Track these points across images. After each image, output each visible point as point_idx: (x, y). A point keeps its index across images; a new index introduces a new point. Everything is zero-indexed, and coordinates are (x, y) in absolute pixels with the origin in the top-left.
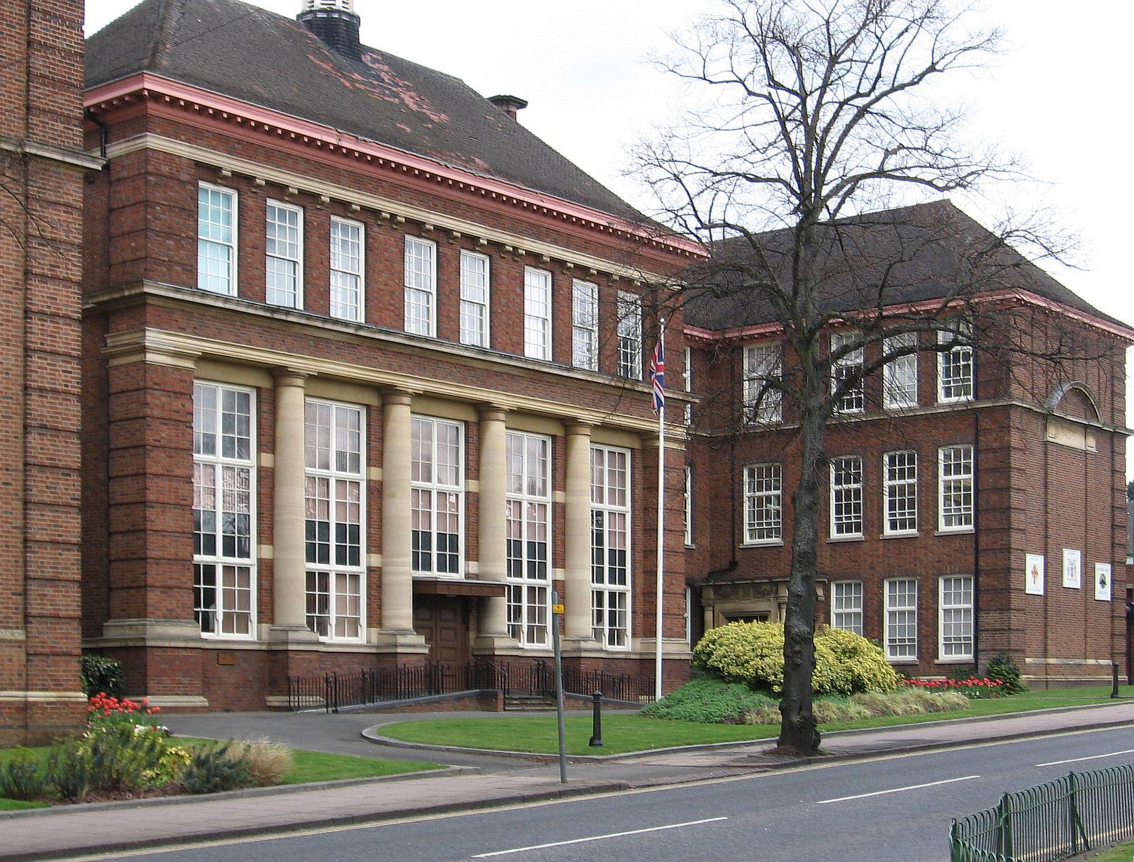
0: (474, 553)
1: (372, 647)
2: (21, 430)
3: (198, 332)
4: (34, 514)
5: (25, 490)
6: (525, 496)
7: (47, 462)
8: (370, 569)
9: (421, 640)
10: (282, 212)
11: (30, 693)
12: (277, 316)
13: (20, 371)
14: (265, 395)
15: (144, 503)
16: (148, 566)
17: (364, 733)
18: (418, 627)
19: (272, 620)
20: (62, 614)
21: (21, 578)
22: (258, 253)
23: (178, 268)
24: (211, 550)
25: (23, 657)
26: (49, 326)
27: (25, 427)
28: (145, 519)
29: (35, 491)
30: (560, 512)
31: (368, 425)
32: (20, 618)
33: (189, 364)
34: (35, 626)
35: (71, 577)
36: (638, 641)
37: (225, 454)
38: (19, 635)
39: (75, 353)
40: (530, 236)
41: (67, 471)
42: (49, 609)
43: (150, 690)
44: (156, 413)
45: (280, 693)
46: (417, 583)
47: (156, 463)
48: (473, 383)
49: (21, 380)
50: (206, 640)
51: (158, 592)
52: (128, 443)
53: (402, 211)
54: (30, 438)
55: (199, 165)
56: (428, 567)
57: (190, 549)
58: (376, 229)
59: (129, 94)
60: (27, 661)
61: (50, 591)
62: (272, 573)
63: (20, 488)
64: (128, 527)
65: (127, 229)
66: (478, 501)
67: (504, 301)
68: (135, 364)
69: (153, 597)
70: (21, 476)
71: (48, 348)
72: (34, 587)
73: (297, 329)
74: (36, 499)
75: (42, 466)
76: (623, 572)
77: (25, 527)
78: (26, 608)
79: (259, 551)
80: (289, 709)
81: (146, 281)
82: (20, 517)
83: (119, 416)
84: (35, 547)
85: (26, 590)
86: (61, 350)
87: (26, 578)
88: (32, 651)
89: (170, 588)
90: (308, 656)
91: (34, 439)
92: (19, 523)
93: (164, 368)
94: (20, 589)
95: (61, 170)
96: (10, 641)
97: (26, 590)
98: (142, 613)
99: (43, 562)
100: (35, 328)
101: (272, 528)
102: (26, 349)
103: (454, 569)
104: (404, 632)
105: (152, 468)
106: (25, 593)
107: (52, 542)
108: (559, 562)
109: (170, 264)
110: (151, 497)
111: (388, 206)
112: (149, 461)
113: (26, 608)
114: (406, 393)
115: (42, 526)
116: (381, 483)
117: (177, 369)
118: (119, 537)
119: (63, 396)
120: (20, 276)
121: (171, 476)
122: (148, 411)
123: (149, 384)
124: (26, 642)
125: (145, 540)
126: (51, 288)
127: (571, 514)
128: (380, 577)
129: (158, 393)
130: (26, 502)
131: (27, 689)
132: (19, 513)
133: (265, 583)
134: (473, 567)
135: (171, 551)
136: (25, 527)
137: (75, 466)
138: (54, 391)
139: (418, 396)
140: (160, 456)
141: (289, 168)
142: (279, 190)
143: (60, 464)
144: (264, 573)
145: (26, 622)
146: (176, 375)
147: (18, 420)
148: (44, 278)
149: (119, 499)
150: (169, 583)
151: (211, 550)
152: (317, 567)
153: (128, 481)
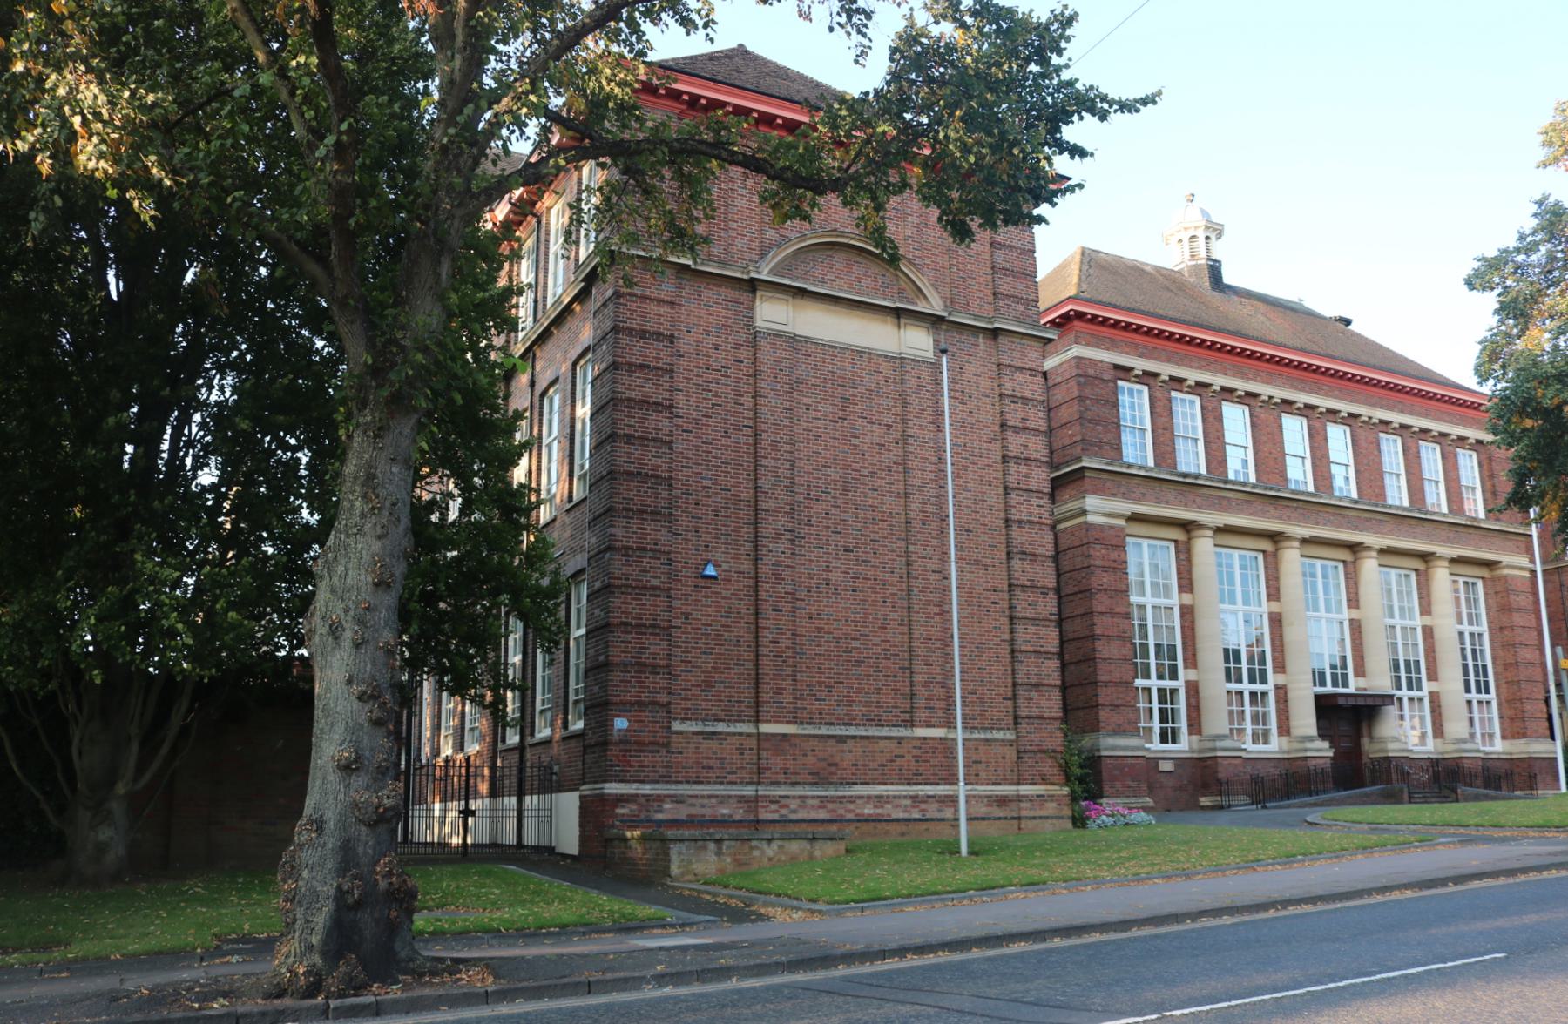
0: (1360, 672)
1: (1284, 752)
2: (1004, 557)
3: (1126, 496)
4: (1020, 628)
5: (1010, 608)
6: (1397, 621)
7: (1028, 583)
8: (1277, 687)
9: (1326, 745)
10: (1183, 400)
11: (1021, 787)
12: (1188, 480)
13: (1001, 507)
14: (1181, 547)
15: (1092, 637)
16: (1099, 689)
17: (1308, 819)
18: (1322, 735)
19: (1199, 732)
20: (1046, 715)
21: (1010, 685)
22: (1168, 434)
23: (1107, 447)
24: (1147, 676)
25: (1014, 755)
26: (1023, 469)
27: (1008, 553)
28: (1094, 650)
29: (1019, 609)
30: (1428, 632)
31: (1266, 567)
32: (1011, 720)
33: (1121, 522)
34: (1024, 727)
35: (1053, 682)
36: (1507, 743)
37: (1153, 596)
38: (1010, 735)
39: (1046, 490)
40: (1381, 407)
41: (1044, 591)
42: (1035, 712)
43: (1105, 794)
44: (1098, 563)
45: (1212, 794)
46: (1319, 699)
47: (1100, 603)
48: (1348, 528)
49: (1002, 515)
50: (1148, 749)
51: (1107, 709)
52: (1076, 589)
53: (1279, 393)
54: (1013, 562)
55: (1117, 367)
56: (1323, 684)
57: (1132, 673)
58: (1258, 409)
59: (1059, 317)
60: (1019, 758)
61: (1035, 695)
62: (1197, 693)
63: (1006, 606)
64: (1079, 657)
65: (1064, 421)
66: (1360, 626)
67: (1365, 462)
68: (1079, 525)
69: (1103, 714)
70: (1006, 596)
71: (1024, 487)
72: (1022, 694)
73: (1205, 491)
74: (1020, 615)
75: (1023, 586)
76: (1486, 683)
77: (1012, 640)
78: (1015, 711)
79: (1185, 675)
80: (1221, 807)
81: (1084, 458)
82: (1008, 631)
83: (1067, 569)
84: (1021, 657)
85: (1015, 695)
86: (1034, 488)
87: (1015, 684)
88: (1022, 749)
89: (1117, 706)
90: (1234, 761)
91: (1016, 564)
92: (1007, 637)
93: (1102, 527)
94: (1010, 695)
95: (1024, 341)
96: (1003, 740)
97: (1015, 695)
98: (1095, 728)
99: (1029, 669)
100: (1012, 471)
101: (1194, 655)
102: (1006, 488)
103: (1345, 685)
104: (1310, 739)
105: (1098, 608)
106: (1014, 698)
107: (1035, 652)
108: (1433, 676)
109: (1100, 444)
110: (1098, 631)
111: (1265, 390)
112: (1095, 602)
113: (1015, 711)
114: (1296, 539)
115: (1026, 637)
116: (1280, 615)
117: (1112, 527)
118: (1072, 667)
119: (1038, 526)
120: (997, 428)
121: (1112, 613)
122: (1092, 562)
123: (1091, 540)
124: (1017, 741)
125: (1095, 667)
126: (1022, 438)
127: (1438, 634)
128: (1286, 693)
129: (1098, 547)
130: (1011, 618)
131: (1019, 784)
132: (1006, 629)
133: (1193, 701)
134: (1362, 683)
135: (1116, 676)
136: (1012, 640)
137: (1051, 585)
138: (1029, 522)
139: (1305, 541)
140: (1104, 598)
141: (1187, 366)
142: (1177, 382)
143: (1039, 584)
144: (1192, 693)
145: (1016, 723)
146: (1112, 532)
147: (1002, 549)
148: (1016, 429)
149: (1071, 636)
150: (1116, 703)
151: (1147, 676)
152: (1234, 686)
153: (1078, 620)
